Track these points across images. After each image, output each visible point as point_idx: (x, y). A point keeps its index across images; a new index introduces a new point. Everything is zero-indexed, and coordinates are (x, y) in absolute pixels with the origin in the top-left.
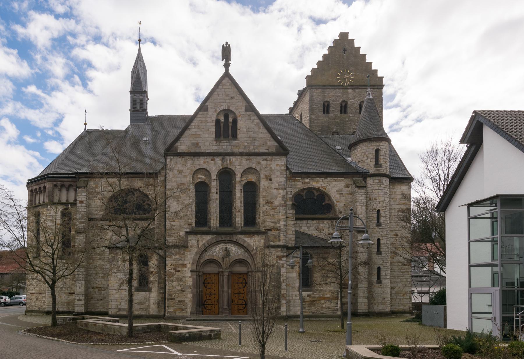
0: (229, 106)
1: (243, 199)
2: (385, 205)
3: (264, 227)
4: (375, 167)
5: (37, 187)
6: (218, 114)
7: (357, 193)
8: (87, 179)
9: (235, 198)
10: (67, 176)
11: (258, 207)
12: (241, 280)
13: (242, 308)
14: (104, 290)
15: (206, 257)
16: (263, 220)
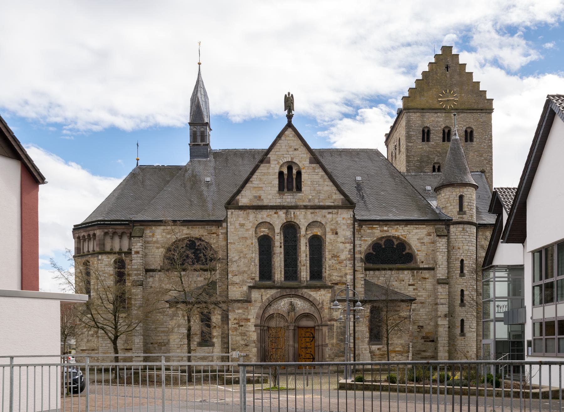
0: (292, 158)
1: (308, 253)
2: (469, 254)
3: (330, 281)
4: (459, 214)
5: (86, 234)
6: (281, 166)
7: (438, 243)
8: (142, 227)
10: (120, 222)
11: (324, 260)
12: (308, 335)
14: (165, 345)
15: (271, 311)
16: (329, 274)
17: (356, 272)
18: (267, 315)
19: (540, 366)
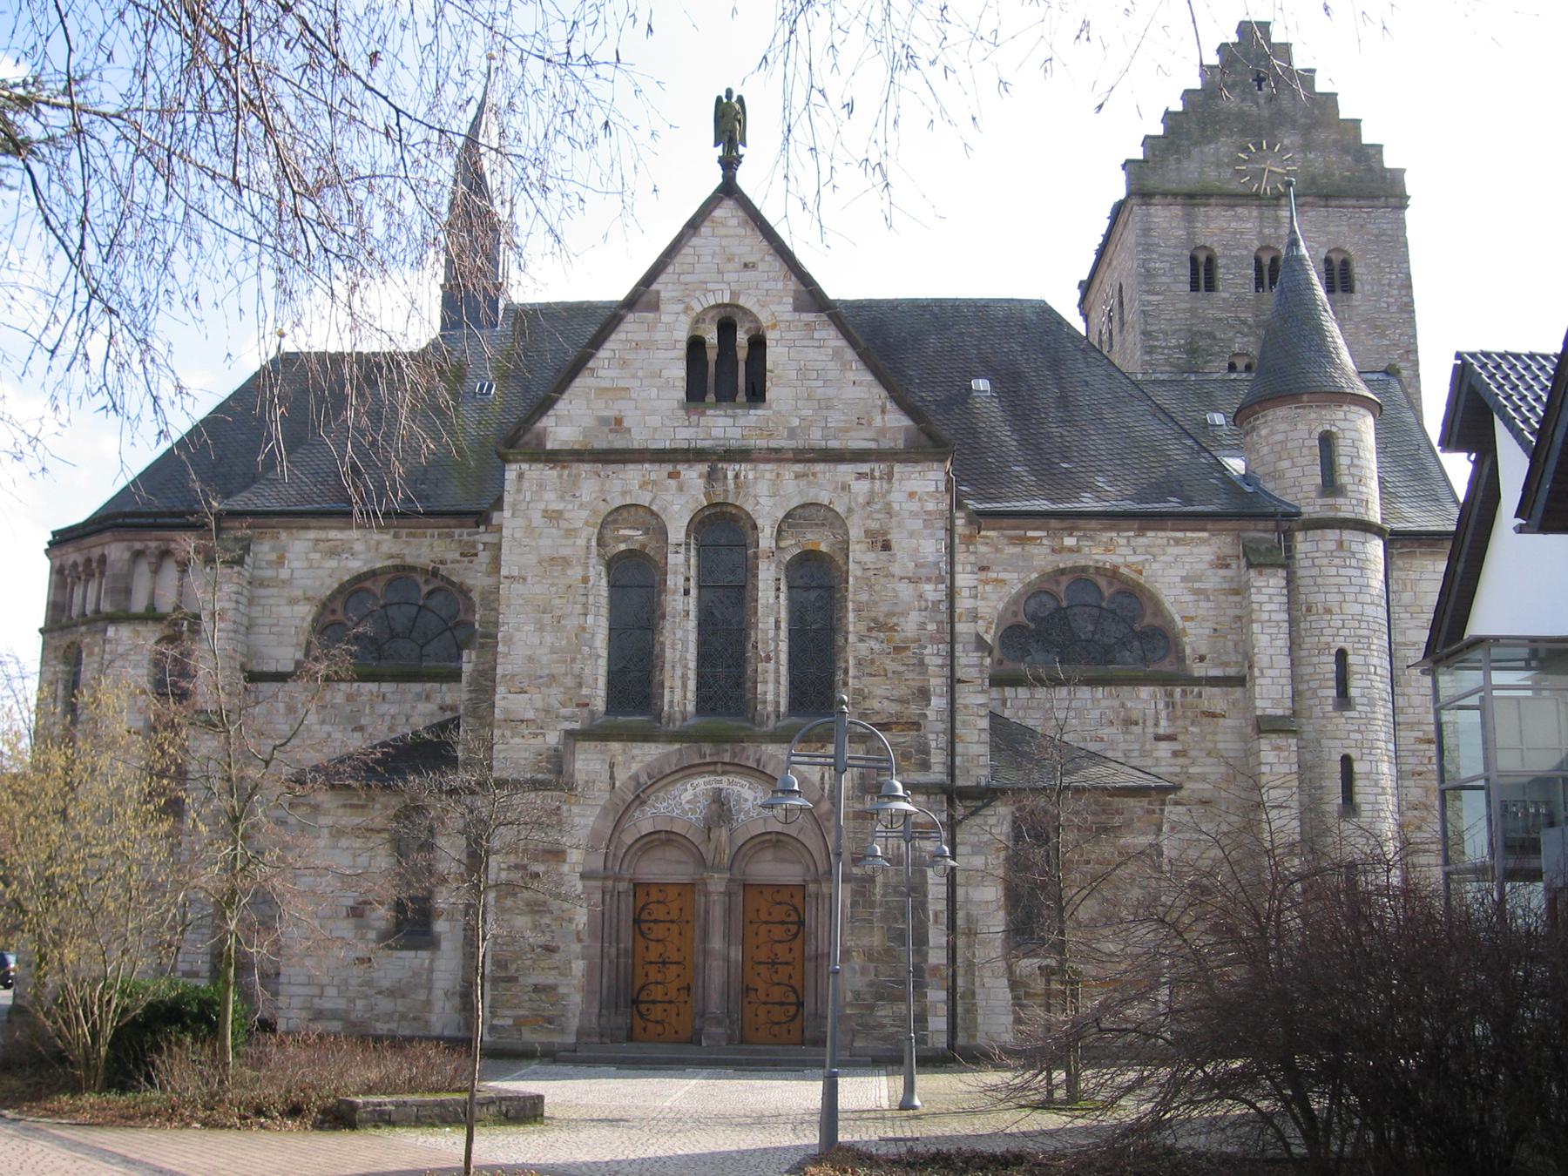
1: (784, 615)
2: (1364, 632)
6: (698, 321)
9: (756, 613)
11: (841, 642)
13: (784, 1019)
17: (958, 687)
18: (628, 839)
19: (959, 681)
